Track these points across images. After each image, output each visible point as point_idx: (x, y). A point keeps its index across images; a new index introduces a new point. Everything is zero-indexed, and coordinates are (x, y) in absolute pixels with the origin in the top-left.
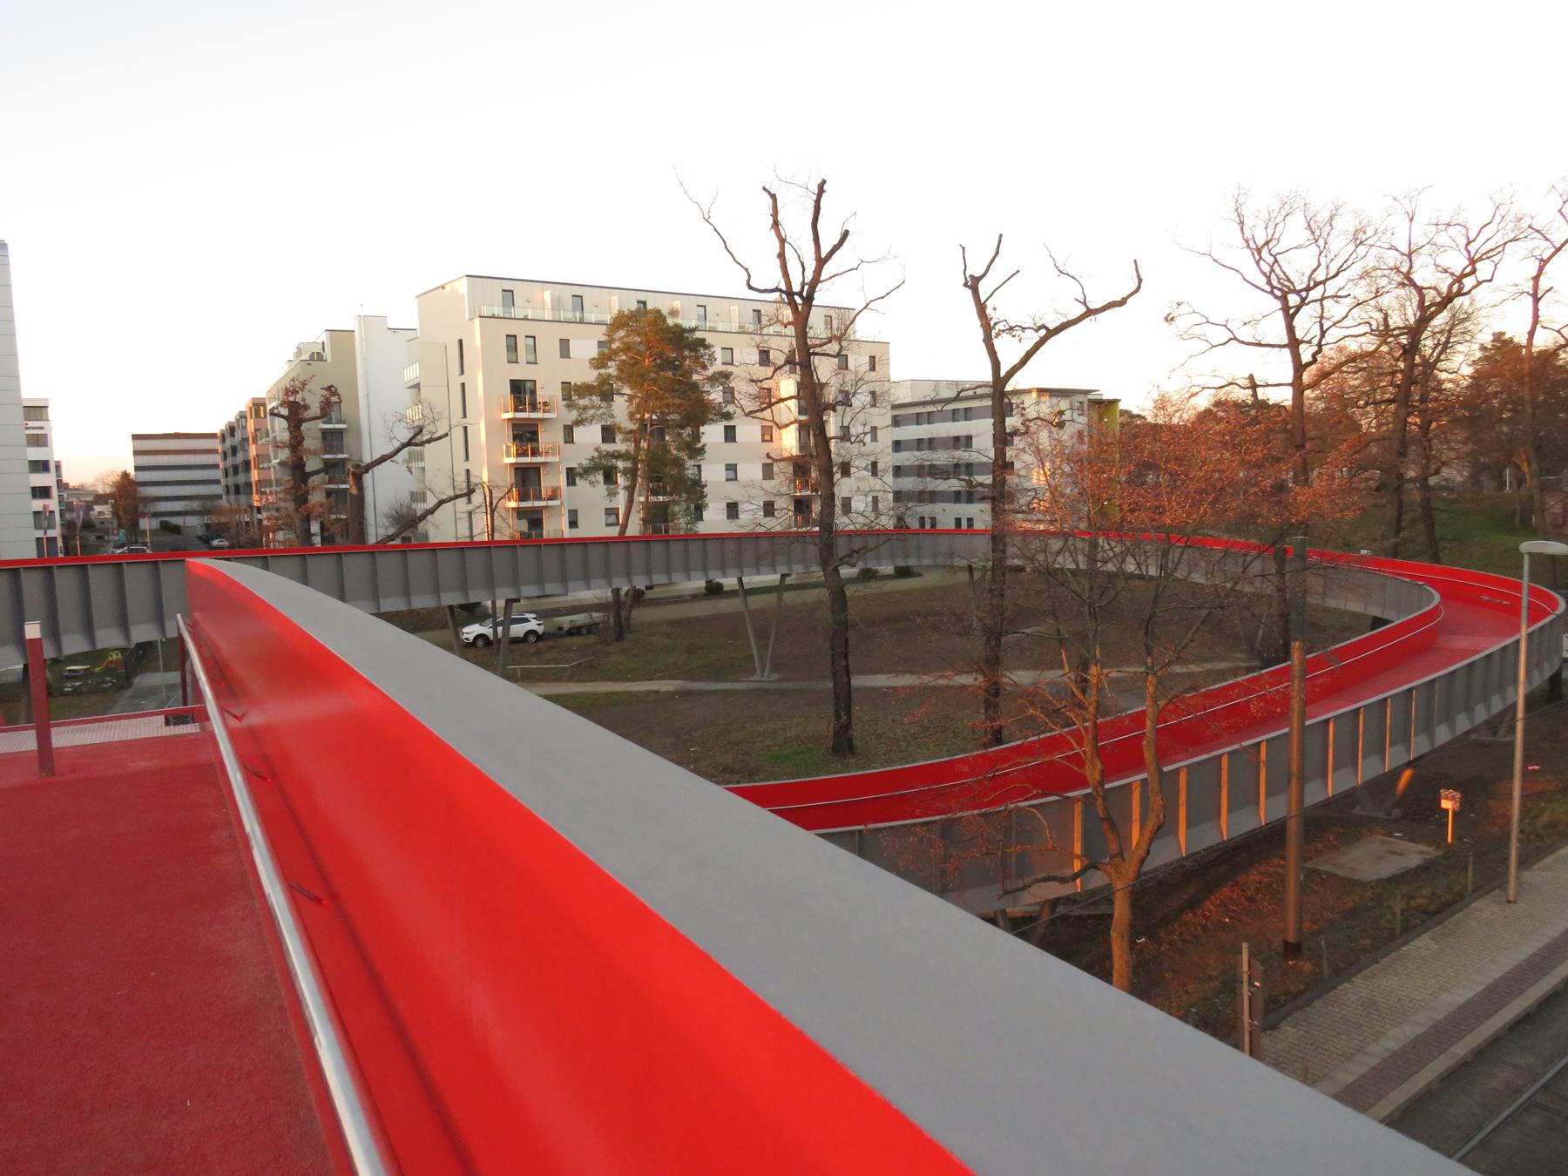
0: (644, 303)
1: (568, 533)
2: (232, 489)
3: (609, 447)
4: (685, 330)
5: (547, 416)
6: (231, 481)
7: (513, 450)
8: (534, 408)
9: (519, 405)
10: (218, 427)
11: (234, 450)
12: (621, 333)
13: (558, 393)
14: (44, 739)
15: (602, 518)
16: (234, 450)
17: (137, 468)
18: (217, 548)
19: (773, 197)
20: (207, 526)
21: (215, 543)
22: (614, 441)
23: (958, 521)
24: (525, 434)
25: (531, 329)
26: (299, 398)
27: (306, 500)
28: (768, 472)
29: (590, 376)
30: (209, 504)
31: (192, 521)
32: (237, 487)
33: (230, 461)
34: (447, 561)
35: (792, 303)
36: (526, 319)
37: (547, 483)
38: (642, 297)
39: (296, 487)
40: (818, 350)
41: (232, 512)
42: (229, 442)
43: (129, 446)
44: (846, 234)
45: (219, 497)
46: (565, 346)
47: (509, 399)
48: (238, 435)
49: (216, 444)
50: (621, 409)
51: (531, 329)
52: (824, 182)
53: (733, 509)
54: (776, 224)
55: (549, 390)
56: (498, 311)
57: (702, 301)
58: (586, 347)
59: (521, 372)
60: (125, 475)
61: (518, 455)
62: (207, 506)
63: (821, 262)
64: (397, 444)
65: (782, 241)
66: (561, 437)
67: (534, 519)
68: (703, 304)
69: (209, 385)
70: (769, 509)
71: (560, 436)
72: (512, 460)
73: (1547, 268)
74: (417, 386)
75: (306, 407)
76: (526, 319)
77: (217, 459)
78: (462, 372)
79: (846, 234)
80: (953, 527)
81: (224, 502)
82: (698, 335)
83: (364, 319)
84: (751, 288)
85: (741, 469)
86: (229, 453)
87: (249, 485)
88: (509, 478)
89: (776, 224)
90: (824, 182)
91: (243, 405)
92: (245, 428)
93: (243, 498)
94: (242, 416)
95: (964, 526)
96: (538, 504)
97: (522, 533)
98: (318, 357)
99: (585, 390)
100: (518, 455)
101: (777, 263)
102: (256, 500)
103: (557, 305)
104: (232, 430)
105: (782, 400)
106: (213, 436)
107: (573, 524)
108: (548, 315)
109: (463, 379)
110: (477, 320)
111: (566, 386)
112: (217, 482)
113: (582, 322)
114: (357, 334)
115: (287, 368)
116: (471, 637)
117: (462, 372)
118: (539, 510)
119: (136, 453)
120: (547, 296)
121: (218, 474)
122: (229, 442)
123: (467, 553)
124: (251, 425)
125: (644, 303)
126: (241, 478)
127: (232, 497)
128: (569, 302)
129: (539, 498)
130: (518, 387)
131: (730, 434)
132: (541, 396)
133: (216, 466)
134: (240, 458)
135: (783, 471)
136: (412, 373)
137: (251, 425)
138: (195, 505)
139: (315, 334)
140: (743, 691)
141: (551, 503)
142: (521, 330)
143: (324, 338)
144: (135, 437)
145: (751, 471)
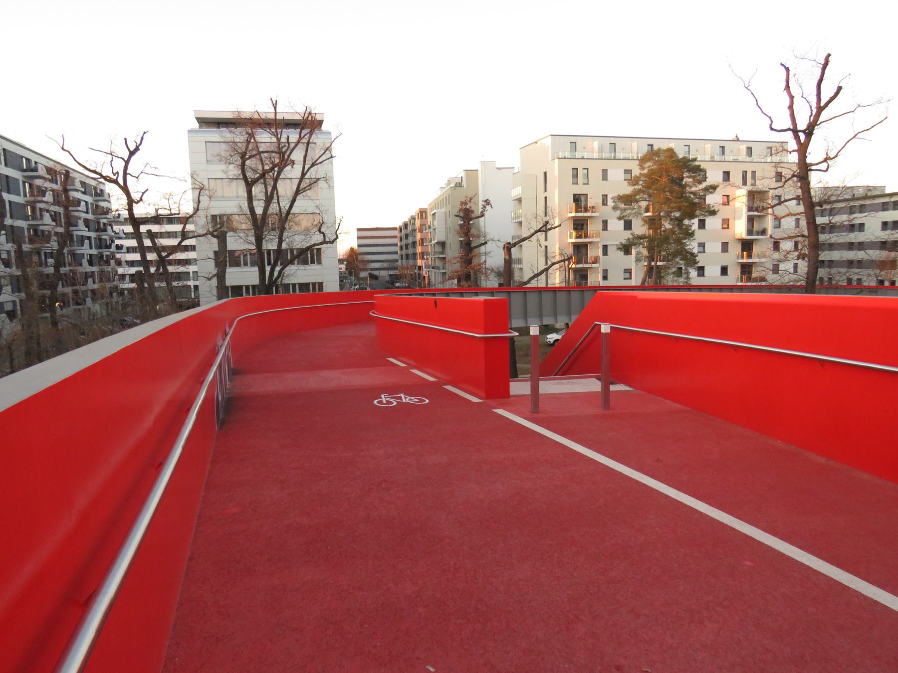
0: (652, 146)
1: (603, 283)
2: (404, 257)
4: (689, 161)
5: (593, 214)
6: (404, 252)
7: (574, 234)
8: (586, 210)
9: (578, 208)
10: (398, 224)
11: (407, 236)
12: (649, 164)
14: (535, 388)
15: (622, 275)
16: (407, 236)
17: (359, 246)
18: (398, 287)
19: (787, 69)
20: (390, 276)
21: (397, 285)
23: (850, 281)
24: (580, 225)
25: (585, 164)
26: (468, 207)
27: (471, 263)
28: (725, 247)
30: (392, 265)
31: (384, 273)
32: (407, 256)
33: (404, 242)
34: (532, 298)
35: (797, 137)
36: (583, 158)
37: (591, 253)
38: (651, 142)
39: (467, 255)
40: (813, 168)
41: (403, 268)
42: (404, 232)
43: (355, 234)
44: (840, 89)
45: (397, 261)
47: (573, 205)
48: (410, 228)
49: (397, 233)
51: (585, 164)
52: (829, 55)
54: (787, 87)
55: (594, 200)
56: (567, 155)
57: (687, 143)
58: (617, 175)
59: (579, 189)
60: (352, 249)
61: (577, 237)
62: (391, 265)
63: (820, 109)
64: (532, 231)
65: (792, 98)
66: (600, 226)
67: (582, 275)
68: (688, 143)
70: (724, 271)
71: (600, 226)
72: (573, 240)
73: (133, 158)
74: (520, 200)
75: (472, 212)
76: (583, 158)
77: (397, 241)
78: (545, 191)
79: (840, 89)
80: (844, 283)
81: (399, 263)
82: (697, 163)
83: (484, 163)
84: (772, 129)
85: (717, 243)
86: (404, 238)
87: (415, 254)
88: (570, 251)
89: (787, 87)
90: (829, 55)
91: (414, 212)
92: (414, 224)
93: (411, 262)
94: (413, 218)
95: (855, 283)
96: (586, 266)
98: (459, 185)
100: (577, 237)
101: (788, 112)
102: (419, 262)
103: (601, 149)
104: (406, 225)
105: (786, 201)
106: (395, 229)
107: (605, 278)
108: (596, 156)
110: (556, 160)
112: (397, 253)
113: (615, 159)
114: (480, 172)
115: (439, 193)
116: (552, 341)
117: (545, 191)
118: (586, 270)
119: (359, 238)
120: (596, 145)
121: (397, 249)
122: (404, 232)
123: (543, 294)
124: (418, 223)
125: (652, 146)
126: (411, 251)
127: (404, 261)
128: (607, 147)
129: (586, 262)
130: (577, 199)
133: (396, 245)
134: (410, 240)
135: (735, 249)
136: (517, 192)
137: (418, 223)
138: (386, 265)
139: (457, 172)
140: (331, 365)
141: (594, 265)
142: (580, 165)
143: (463, 174)
144: (359, 230)
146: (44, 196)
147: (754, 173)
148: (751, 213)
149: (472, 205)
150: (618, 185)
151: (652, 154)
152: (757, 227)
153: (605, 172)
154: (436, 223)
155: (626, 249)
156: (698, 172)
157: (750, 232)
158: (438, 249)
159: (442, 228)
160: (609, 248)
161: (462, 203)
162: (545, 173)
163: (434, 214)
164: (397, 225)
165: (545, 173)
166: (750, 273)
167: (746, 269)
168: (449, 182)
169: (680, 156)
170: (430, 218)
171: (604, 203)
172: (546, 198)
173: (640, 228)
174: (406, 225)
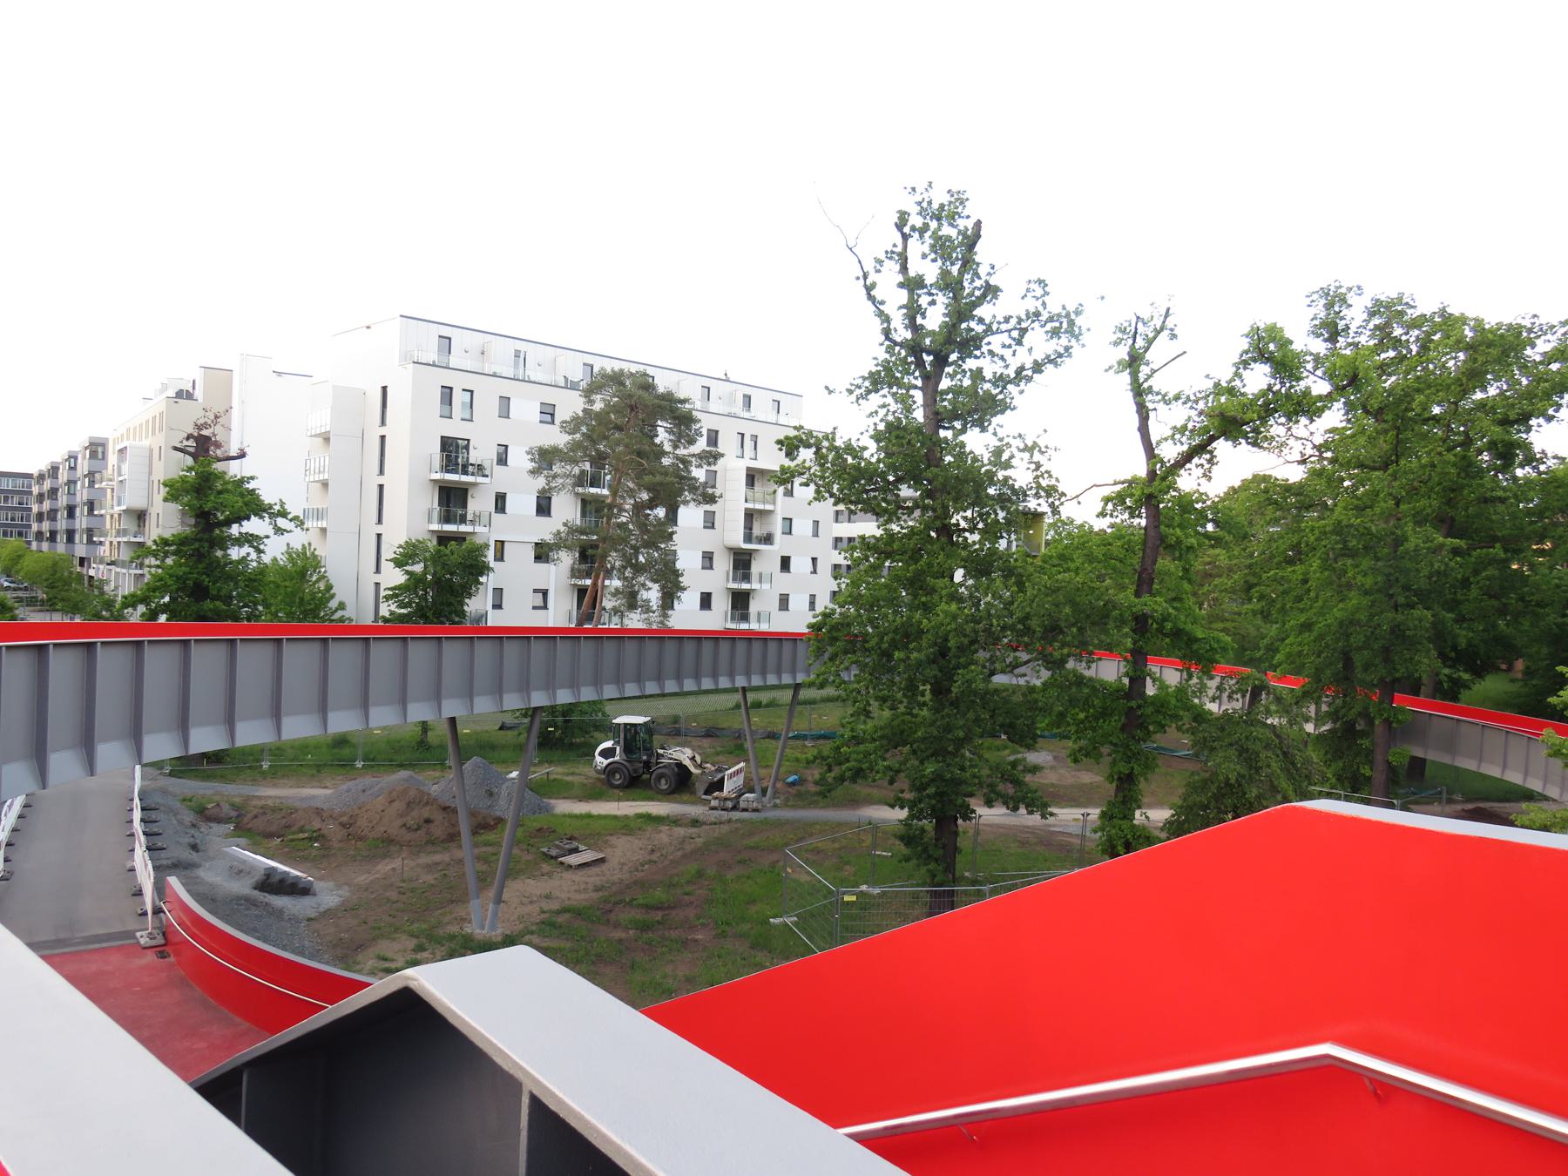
28: (708, 558)
38: (590, 359)
55: (481, 453)
58: (526, 409)
59: (455, 429)
91: (77, 443)
94: (73, 457)
135: (723, 564)
137: (83, 466)
138: (369, 793)
142: (458, 382)
146: (721, 790)
147: (755, 438)
148: (750, 506)
149: (218, 429)
150: (528, 431)
151: (598, 383)
152: (756, 531)
153: (505, 401)
154: (125, 468)
155: (542, 553)
156: (683, 422)
157: (748, 538)
158: (129, 524)
159: (140, 483)
160: (506, 545)
161: (199, 427)
162: (384, 388)
163: (121, 451)
164: (34, 471)
165: (384, 388)
166: (746, 606)
167: (740, 601)
168: (165, 387)
169: (661, 390)
170: (112, 459)
171: (502, 460)
172: (383, 438)
173: (566, 510)
174: (54, 470)
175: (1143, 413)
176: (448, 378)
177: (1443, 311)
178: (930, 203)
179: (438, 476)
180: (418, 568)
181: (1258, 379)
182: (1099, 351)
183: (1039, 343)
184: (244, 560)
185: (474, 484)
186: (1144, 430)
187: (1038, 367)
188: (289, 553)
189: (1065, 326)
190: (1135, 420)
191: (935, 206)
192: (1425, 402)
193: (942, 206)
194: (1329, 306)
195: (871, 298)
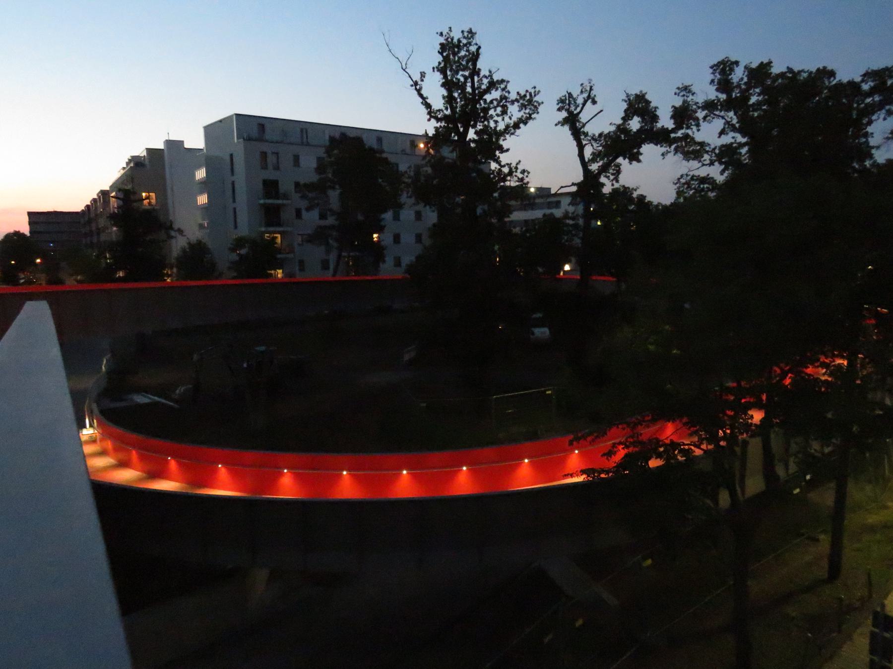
3: (323, 223)
13: (292, 187)
22: (326, 219)
29: (314, 178)
46: (296, 159)
50: (334, 195)
53: (398, 263)
55: (286, 186)
58: (309, 162)
59: (270, 175)
69: (650, 99)
82: (384, 155)
97: (635, 157)
99: (310, 187)
109: (233, 178)
111: (297, 185)
115: (122, 172)
131: (396, 218)
132: (282, 188)
145: (408, 238)
175: (581, 148)
176: (265, 147)
177: (790, 70)
178: (452, 39)
179: (262, 202)
180: (243, 251)
181: (635, 124)
182: (549, 113)
183: (515, 112)
184: (603, 185)
185: (284, 205)
186: (581, 155)
187: (516, 126)
188: (189, 244)
189: (529, 102)
190: (576, 150)
191: (455, 40)
192: (790, 119)
193: (459, 41)
194: (723, 72)
195: (421, 96)
